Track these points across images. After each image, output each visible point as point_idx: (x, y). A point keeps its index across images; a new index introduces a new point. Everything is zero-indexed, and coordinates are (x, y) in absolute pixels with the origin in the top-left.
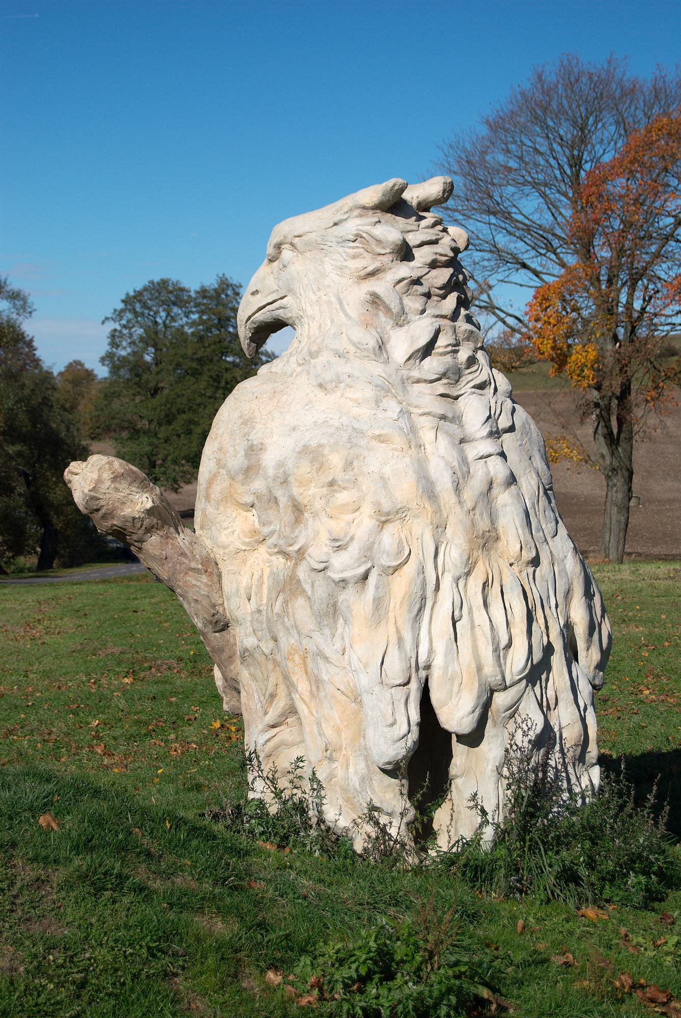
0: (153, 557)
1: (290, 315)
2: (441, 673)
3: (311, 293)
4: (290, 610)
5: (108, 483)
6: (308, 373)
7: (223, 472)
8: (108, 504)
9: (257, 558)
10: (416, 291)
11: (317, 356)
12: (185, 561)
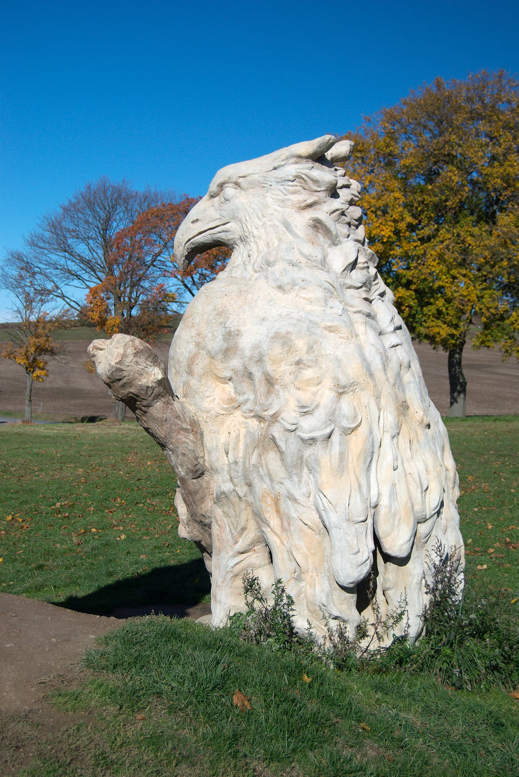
0: (155, 420)
1: (232, 237)
2: (387, 510)
3: (256, 220)
4: (263, 462)
5: (131, 358)
6: (266, 278)
7: (203, 352)
8: (129, 375)
9: (233, 421)
10: (344, 220)
11: (274, 265)
12: (180, 423)
